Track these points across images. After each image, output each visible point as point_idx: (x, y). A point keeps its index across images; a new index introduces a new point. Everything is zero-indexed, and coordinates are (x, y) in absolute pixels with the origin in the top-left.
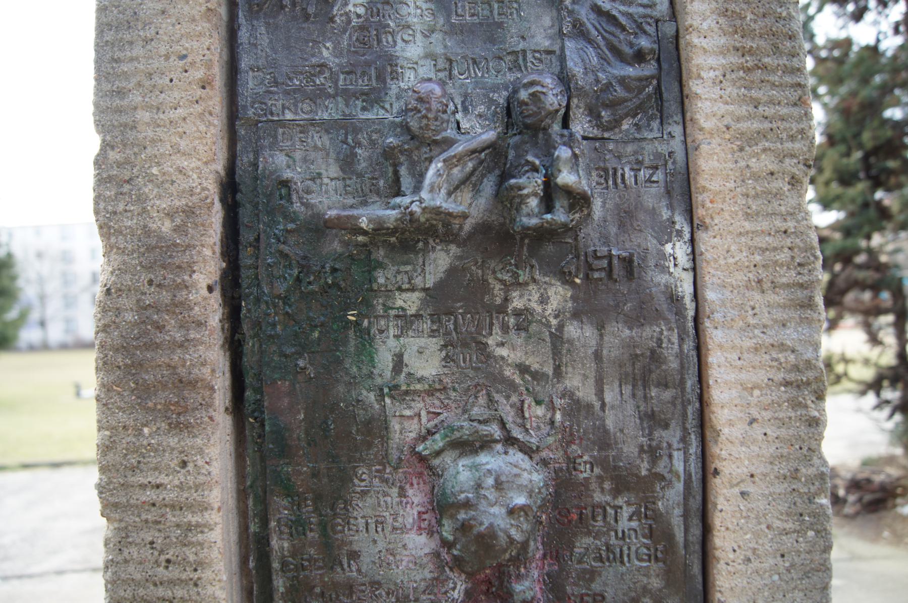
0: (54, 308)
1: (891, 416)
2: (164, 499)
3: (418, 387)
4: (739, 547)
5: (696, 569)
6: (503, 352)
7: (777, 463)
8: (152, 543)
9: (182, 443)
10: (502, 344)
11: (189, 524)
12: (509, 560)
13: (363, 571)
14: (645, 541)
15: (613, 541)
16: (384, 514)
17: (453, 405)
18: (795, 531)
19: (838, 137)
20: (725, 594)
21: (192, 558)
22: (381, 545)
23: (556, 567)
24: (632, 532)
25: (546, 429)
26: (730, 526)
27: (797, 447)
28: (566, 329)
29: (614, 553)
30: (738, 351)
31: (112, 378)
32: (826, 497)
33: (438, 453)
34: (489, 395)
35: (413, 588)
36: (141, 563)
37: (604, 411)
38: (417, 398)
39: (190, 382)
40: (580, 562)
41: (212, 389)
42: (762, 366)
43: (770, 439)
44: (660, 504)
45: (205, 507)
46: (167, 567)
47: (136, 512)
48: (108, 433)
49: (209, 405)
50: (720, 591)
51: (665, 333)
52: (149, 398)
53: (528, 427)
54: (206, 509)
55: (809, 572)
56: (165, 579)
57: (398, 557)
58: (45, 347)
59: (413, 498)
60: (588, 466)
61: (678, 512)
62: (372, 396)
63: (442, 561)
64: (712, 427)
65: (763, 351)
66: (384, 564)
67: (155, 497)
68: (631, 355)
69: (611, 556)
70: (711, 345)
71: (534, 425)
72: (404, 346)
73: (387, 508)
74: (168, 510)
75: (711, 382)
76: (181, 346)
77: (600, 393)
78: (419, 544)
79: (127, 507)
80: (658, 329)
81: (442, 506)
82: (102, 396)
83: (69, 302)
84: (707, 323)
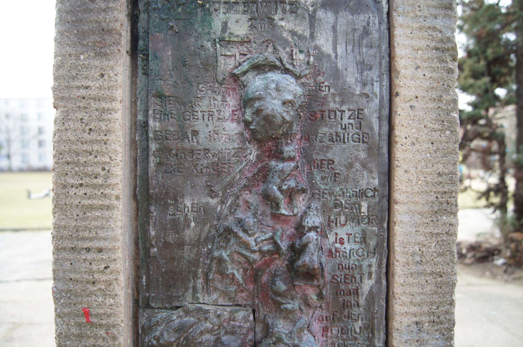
0: (15, 147)
1: (494, 211)
2: (90, 95)
3: (235, 39)
4: (409, 136)
5: (385, 150)
6: (283, 23)
7: (430, 91)
8: (82, 119)
9: (102, 64)
10: (282, 19)
11: (104, 109)
12: (282, 135)
13: (200, 142)
14: (357, 131)
15: (339, 130)
16: (213, 110)
17: (254, 51)
18: (439, 130)
20: (401, 162)
21: (104, 128)
22: (211, 128)
23: (308, 145)
24: (354, 266)
25: (304, 67)
26: (404, 124)
27: (442, 84)
28: (317, 13)
29: (340, 137)
30: (411, 29)
31: (64, 28)
32: (456, 113)
33: (245, 73)
34: (274, 46)
35: (228, 153)
36: (75, 131)
37: (337, 59)
38: (234, 46)
39: (108, 31)
40: (321, 142)
41: (120, 35)
42: (423, 38)
43: (426, 78)
44: (366, 110)
45: (112, 100)
46: (89, 134)
47: (74, 102)
48: (60, 58)
49: (119, 44)
50: (398, 160)
51: (371, 18)
52: (85, 39)
53: (295, 64)
54: (114, 100)
55: (446, 154)
56: (88, 140)
57: (220, 135)
58: (10, 170)
59: (230, 102)
60: (327, 88)
61: (375, 115)
62: (209, 45)
63: (244, 138)
64: (395, 70)
65: (424, 30)
66: (212, 139)
67: (85, 93)
68: (352, 29)
69: (338, 139)
70: (396, 24)
71: (298, 64)
72: (228, 18)
73: (215, 106)
74: (92, 101)
75: (395, 45)
76: (104, 11)
77: (335, 49)
78: (232, 128)
79: (69, 99)
80: (367, 16)
81: (246, 102)
82: (58, 38)
83: (25, 144)
84: (394, 14)
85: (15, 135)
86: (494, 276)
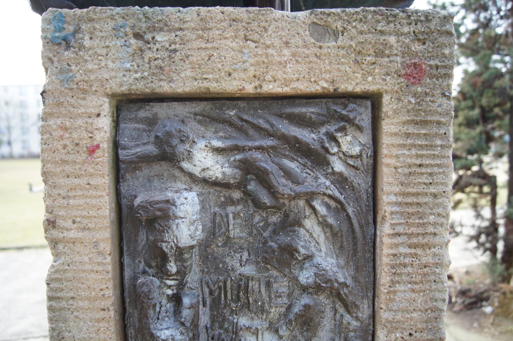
0: (16, 135)
19: (468, 95)
58: (11, 157)
83: (25, 131)
85: (15, 122)
86: (481, 329)
